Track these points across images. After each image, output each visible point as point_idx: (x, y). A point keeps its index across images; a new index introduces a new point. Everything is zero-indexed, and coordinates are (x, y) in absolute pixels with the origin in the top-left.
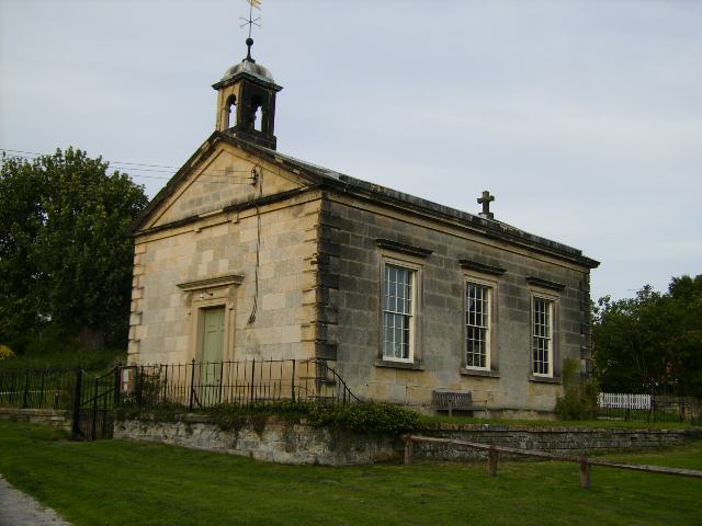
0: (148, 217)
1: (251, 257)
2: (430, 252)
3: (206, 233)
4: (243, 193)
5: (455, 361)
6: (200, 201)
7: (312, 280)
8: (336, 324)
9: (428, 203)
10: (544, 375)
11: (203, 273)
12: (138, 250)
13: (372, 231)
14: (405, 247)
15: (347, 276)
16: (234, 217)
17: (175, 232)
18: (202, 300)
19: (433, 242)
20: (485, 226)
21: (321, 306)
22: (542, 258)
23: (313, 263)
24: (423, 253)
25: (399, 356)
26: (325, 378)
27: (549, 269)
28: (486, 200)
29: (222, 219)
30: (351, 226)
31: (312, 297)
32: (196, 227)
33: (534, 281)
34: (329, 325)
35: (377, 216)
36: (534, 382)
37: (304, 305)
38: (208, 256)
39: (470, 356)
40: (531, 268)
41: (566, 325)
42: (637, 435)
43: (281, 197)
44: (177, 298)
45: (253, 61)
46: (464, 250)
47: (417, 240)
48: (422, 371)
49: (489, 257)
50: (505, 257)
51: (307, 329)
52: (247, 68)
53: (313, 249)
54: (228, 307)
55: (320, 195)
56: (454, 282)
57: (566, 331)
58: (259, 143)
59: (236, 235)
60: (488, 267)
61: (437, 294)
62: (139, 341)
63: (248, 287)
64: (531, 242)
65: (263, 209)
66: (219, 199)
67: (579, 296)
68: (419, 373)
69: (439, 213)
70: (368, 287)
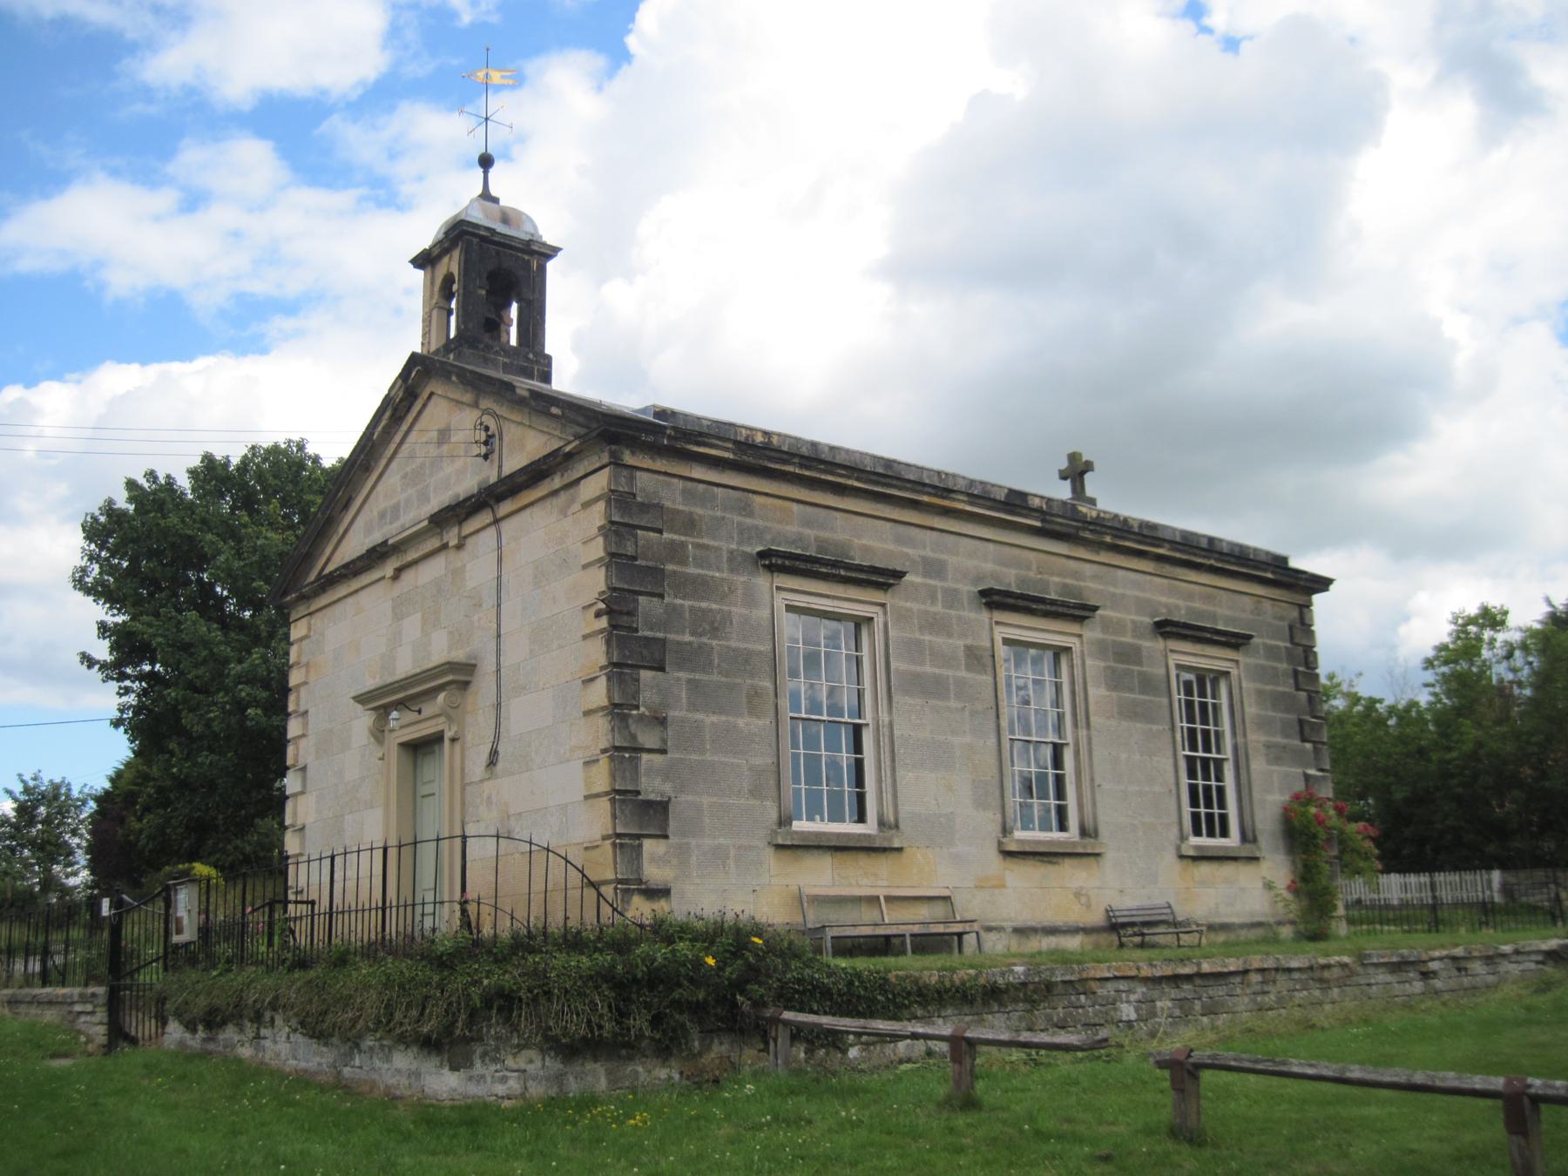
0: (308, 558)
1: (486, 618)
2: (899, 575)
3: (408, 577)
4: (466, 477)
5: (989, 822)
6: (396, 510)
7: (597, 653)
8: (663, 751)
9: (889, 463)
10: (849, 828)
11: (405, 666)
12: (297, 631)
13: (745, 533)
14: (835, 564)
15: (687, 638)
16: (452, 537)
17: (355, 584)
18: (404, 726)
19: (910, 551)
20: (1039, 510)
21: (618, 711)
22: (1193, 576)
23: (598, 615)
24: (882, 578)
25: (1045, 827)
26: (640, 882)
27: (1208, 598)
28: (1077, 471)
29: (433, 543)
30: (690, 525)
31: (599, 694)
32: (388, 569)
33: (1167, 628)
34: (645, 757)
35: (759, 499)
36: (1194, 859)
37: (587, 713)
38: (412, 626)
39: (1196, 818)
40: (1163, 599)
41: (1263, 724)
42: (1434, 966)
43: (535, 474)
44: (364, 720)
45: (495, 200)
46: (989, 567)
47: (866, 549)
48: (900, 850)
49: (1056, 579)
50: (1096, 577)
51: (594, 769)
52: (478, 216)
53: (597, 582)
54: (448, 735)
55: (606, 459)
56: (969, 642)
57: (1263, 738)
58: (507, 368)
59: (458, 573)
60: (1053, 602)
61: (928, 669)
62: (303, 828)
63: (484, 685)
64: (1158, 541)
65: (505, 507)
66: (428, 500)
67: (1290, 657)
68: (892, 856)
69: (919, 485)
70: (742, 661)
